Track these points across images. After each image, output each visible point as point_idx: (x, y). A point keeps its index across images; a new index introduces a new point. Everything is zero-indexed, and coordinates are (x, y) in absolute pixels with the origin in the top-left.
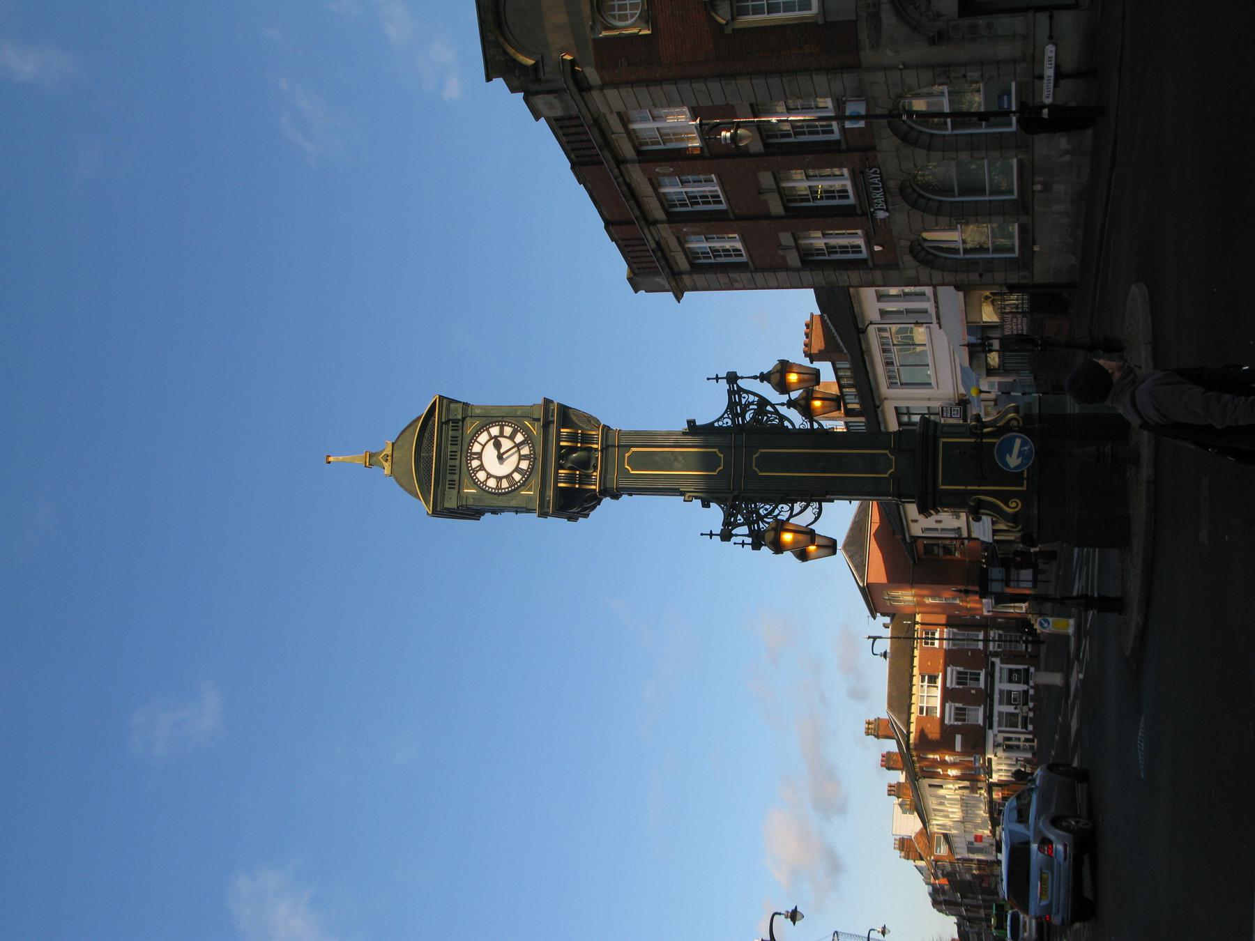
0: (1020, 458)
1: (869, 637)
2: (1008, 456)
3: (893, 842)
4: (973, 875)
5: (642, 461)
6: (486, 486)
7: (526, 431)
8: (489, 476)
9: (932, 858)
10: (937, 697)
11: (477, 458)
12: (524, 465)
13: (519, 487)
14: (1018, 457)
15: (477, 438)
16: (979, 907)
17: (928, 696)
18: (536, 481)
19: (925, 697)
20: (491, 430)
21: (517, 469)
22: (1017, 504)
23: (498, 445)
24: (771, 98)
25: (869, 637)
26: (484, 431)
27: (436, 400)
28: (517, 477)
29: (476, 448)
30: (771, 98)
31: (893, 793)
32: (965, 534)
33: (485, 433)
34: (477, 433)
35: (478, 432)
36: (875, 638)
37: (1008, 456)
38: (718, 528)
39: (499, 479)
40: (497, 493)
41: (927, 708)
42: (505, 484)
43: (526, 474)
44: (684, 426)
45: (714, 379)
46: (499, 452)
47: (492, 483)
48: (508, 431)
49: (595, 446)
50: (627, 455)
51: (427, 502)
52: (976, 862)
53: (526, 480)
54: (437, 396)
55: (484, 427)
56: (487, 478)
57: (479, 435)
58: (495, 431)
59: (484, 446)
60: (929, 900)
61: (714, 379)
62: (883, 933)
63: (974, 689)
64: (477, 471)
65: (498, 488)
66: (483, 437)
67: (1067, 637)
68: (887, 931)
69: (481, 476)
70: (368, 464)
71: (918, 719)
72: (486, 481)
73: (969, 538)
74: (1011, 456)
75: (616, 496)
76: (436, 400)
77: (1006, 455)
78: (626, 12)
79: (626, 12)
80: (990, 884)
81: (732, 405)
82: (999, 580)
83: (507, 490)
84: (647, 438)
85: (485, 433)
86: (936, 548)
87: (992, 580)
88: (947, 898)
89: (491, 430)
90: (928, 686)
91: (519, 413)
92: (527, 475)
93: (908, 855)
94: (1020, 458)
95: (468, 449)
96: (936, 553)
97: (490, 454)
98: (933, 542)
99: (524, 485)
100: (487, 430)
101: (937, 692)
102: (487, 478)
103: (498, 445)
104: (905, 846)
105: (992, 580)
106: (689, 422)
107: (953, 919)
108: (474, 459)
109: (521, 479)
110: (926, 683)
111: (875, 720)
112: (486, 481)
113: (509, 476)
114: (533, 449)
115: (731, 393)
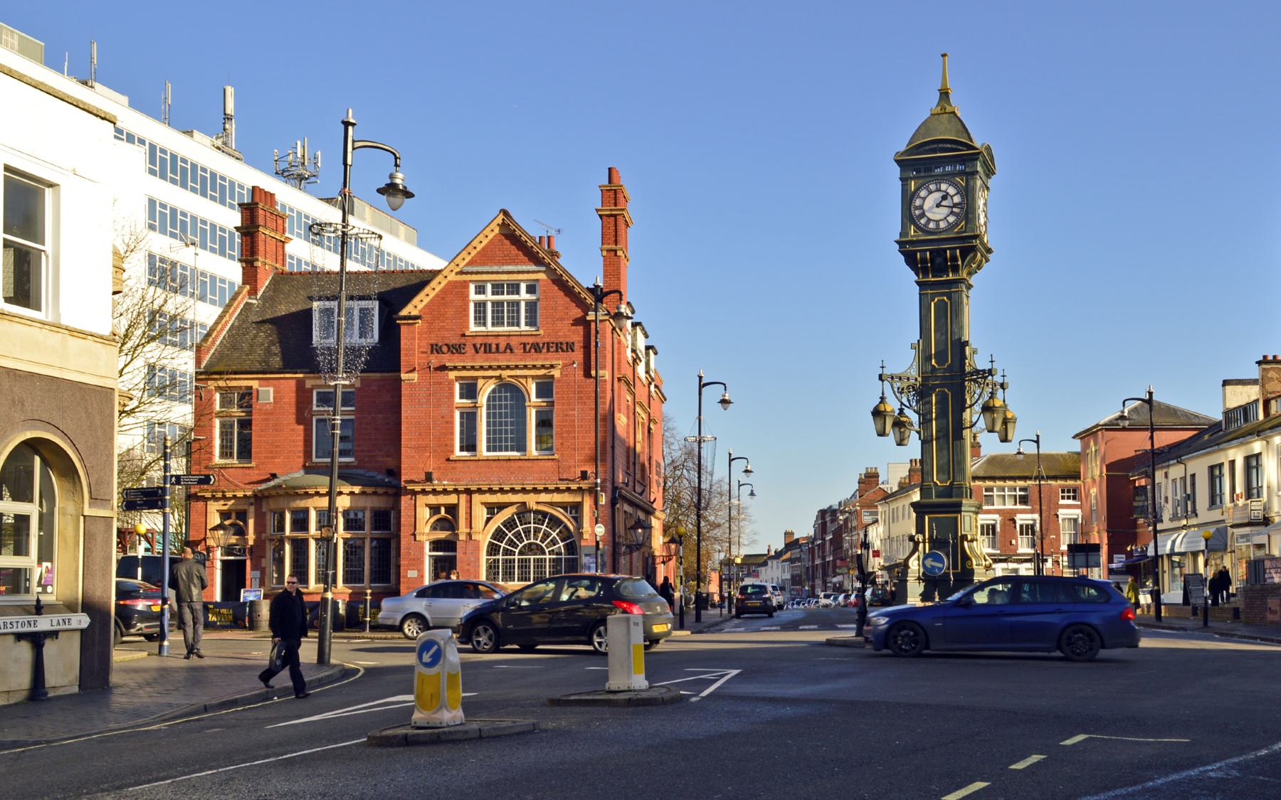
1: (1038, 436)
3: (874, 466)
4: (847, 550)
5: (941, 308)
7: (956, 224)
8: (924, 199)
9: (858, 508)
10: (1005, 505)
14: (931, 566)
16: (824, 558)
17: (1004, 496)
19: (1014, 493)
23: (944, 198)
25: (1038, 436)
28: (923, 221)
31: (914, 464)
32: (1159, 527)
35: (955, 185)
36: (1037, 442)
38: (887, 372)
41: (992, 496)
44: (965, 338)
46: (941, 202)
49: (951, 275)
50: (946, 390)
52: (1156, 588)
60: (825, 507)
62: (747, 471)
63: (1017, 542)
67: (905, 602)
68: (748, 474)
69: (923, 193)
71: (980, 487)
73: (1156, 532)
78: (545, 524)
79: (545, 524)
80: (840, 568)
81: (977, 372)
82: (1087, 558)
84: (957, 311)
86: (1143, 498)
87: (1087, 556)
88: (828, 524)
90: (1015, 496)
91: (970, 216)
93: (863, 483)
96: (1137, 498)
97: (938, 195)
98: (1150, 495)
101: (1009, 505)
103: (944, 198)
104: (870, 479)
105: (1087, 556)
106: (967, 342)
107: (812, 533)
110: (1019, 493)
111: (978, 443)
114: (945, 230)
115: (984, 371)
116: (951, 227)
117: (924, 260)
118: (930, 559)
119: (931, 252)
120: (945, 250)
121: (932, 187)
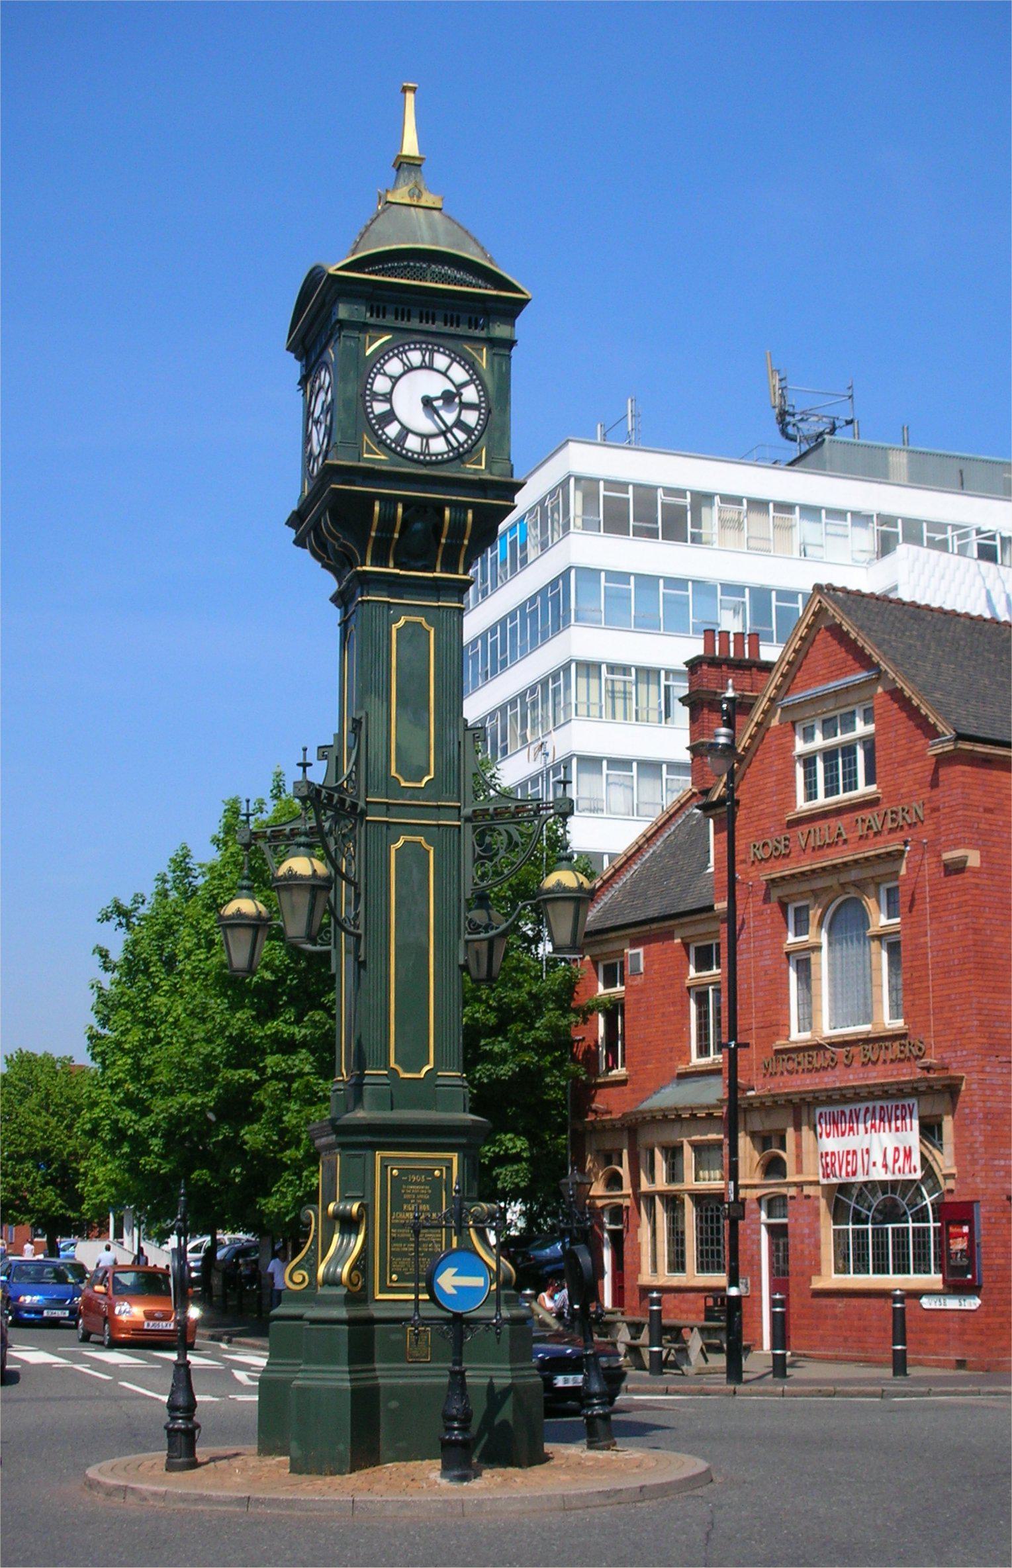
0: (454, 1292)
2: (454, 1270)
6: (376, 375)
8: (395, 380)
11: (424, 360)
12: (413, 443)
13: (375, 433)
14: (455, 1287)
15: (459, 363)
18: (377, 458)
20: (472, 387)
21: (406, 431)
22: (304, 1277)
24: (961, 474)
26: (449, 356)
27: (523, 293)
28: (392, 430)
29: (441, 361)
30: (961, 474)
33: (466, 377)
34: (467, 363)
35: (470, 364)
37: (454, 1270)
39: (388, 397)
40: (365, 395)
42: (379, 408)
43: (398, 445)
45: (304, 771)
47: (381, 384)
48: (471, 418)
51: (344, 268)
53: (388, 447)
54: (530, 297)
55: (476, 377)
56: (391, 377)
57: (463, 367)
58: (470, 394)
59: (445, 374)
61: (304, 771)
64: (402, 360)
65: (375, 396)
66: (459, 374)
69: (394, 366)
70: (402, 160)
72: (385, 374)
74: (455, 1275)
75: (342, 599)
76: (523, 293)
77: (454, 1267)
83: (445, 456)
85: (466, 377)
89: (472, 387)
92: (395, 448)
94: (454, 1292)
95: (439, 346)
97: (435, 385)
99: (381, 443)
100: (432, 352)
102: (391, 377)
103: (448, 397)
108: (424, 356)
109: (388, 437)
112: (385, 374)
113: (390, 417)
116: (460, 455)
117: (387, 522)
118: (451, 1271)
119: (408, 503)
120: (439, 507)
121: (415, 357)
